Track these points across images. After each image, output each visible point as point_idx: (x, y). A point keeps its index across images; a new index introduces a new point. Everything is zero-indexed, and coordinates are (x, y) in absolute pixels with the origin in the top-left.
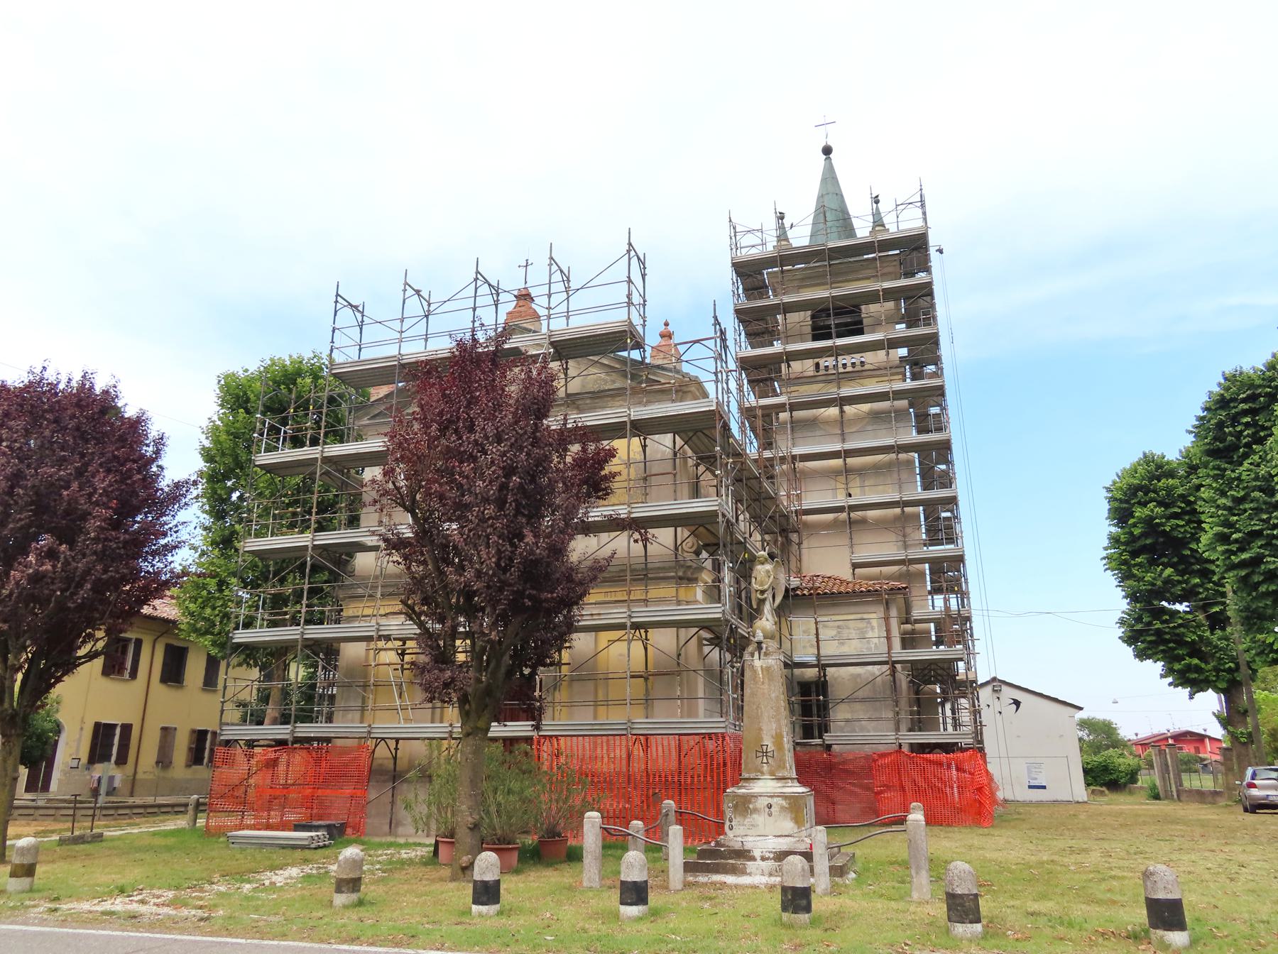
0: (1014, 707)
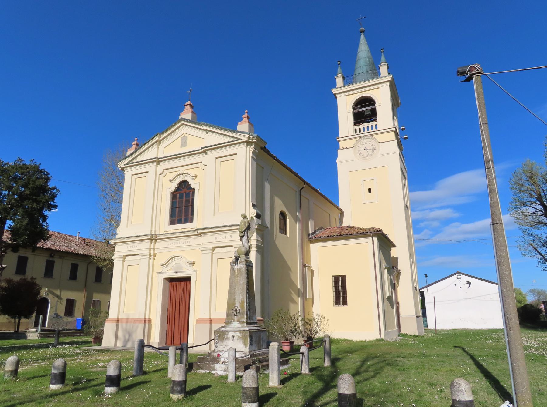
0: (468, 285)
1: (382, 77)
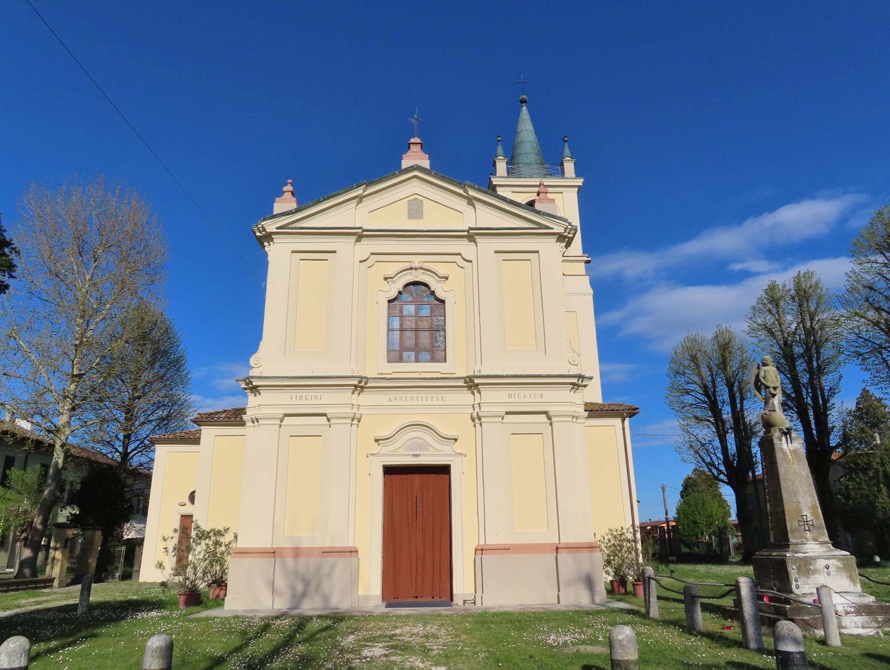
1: (567, 178)
